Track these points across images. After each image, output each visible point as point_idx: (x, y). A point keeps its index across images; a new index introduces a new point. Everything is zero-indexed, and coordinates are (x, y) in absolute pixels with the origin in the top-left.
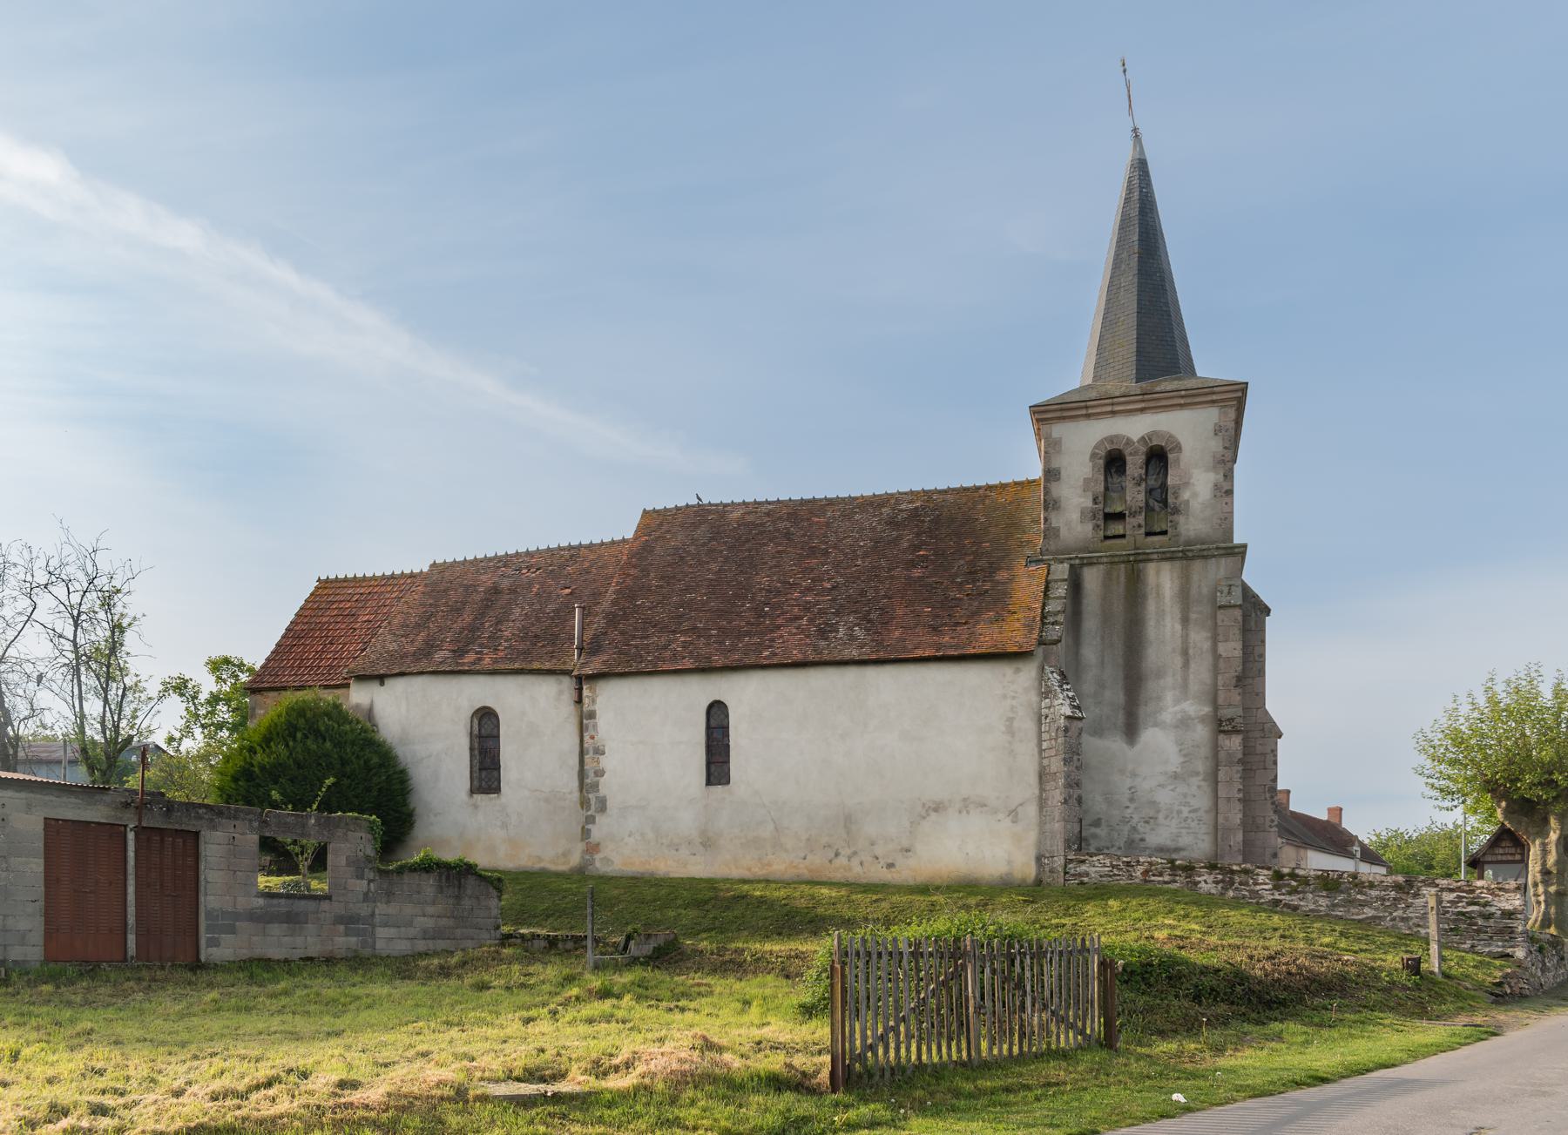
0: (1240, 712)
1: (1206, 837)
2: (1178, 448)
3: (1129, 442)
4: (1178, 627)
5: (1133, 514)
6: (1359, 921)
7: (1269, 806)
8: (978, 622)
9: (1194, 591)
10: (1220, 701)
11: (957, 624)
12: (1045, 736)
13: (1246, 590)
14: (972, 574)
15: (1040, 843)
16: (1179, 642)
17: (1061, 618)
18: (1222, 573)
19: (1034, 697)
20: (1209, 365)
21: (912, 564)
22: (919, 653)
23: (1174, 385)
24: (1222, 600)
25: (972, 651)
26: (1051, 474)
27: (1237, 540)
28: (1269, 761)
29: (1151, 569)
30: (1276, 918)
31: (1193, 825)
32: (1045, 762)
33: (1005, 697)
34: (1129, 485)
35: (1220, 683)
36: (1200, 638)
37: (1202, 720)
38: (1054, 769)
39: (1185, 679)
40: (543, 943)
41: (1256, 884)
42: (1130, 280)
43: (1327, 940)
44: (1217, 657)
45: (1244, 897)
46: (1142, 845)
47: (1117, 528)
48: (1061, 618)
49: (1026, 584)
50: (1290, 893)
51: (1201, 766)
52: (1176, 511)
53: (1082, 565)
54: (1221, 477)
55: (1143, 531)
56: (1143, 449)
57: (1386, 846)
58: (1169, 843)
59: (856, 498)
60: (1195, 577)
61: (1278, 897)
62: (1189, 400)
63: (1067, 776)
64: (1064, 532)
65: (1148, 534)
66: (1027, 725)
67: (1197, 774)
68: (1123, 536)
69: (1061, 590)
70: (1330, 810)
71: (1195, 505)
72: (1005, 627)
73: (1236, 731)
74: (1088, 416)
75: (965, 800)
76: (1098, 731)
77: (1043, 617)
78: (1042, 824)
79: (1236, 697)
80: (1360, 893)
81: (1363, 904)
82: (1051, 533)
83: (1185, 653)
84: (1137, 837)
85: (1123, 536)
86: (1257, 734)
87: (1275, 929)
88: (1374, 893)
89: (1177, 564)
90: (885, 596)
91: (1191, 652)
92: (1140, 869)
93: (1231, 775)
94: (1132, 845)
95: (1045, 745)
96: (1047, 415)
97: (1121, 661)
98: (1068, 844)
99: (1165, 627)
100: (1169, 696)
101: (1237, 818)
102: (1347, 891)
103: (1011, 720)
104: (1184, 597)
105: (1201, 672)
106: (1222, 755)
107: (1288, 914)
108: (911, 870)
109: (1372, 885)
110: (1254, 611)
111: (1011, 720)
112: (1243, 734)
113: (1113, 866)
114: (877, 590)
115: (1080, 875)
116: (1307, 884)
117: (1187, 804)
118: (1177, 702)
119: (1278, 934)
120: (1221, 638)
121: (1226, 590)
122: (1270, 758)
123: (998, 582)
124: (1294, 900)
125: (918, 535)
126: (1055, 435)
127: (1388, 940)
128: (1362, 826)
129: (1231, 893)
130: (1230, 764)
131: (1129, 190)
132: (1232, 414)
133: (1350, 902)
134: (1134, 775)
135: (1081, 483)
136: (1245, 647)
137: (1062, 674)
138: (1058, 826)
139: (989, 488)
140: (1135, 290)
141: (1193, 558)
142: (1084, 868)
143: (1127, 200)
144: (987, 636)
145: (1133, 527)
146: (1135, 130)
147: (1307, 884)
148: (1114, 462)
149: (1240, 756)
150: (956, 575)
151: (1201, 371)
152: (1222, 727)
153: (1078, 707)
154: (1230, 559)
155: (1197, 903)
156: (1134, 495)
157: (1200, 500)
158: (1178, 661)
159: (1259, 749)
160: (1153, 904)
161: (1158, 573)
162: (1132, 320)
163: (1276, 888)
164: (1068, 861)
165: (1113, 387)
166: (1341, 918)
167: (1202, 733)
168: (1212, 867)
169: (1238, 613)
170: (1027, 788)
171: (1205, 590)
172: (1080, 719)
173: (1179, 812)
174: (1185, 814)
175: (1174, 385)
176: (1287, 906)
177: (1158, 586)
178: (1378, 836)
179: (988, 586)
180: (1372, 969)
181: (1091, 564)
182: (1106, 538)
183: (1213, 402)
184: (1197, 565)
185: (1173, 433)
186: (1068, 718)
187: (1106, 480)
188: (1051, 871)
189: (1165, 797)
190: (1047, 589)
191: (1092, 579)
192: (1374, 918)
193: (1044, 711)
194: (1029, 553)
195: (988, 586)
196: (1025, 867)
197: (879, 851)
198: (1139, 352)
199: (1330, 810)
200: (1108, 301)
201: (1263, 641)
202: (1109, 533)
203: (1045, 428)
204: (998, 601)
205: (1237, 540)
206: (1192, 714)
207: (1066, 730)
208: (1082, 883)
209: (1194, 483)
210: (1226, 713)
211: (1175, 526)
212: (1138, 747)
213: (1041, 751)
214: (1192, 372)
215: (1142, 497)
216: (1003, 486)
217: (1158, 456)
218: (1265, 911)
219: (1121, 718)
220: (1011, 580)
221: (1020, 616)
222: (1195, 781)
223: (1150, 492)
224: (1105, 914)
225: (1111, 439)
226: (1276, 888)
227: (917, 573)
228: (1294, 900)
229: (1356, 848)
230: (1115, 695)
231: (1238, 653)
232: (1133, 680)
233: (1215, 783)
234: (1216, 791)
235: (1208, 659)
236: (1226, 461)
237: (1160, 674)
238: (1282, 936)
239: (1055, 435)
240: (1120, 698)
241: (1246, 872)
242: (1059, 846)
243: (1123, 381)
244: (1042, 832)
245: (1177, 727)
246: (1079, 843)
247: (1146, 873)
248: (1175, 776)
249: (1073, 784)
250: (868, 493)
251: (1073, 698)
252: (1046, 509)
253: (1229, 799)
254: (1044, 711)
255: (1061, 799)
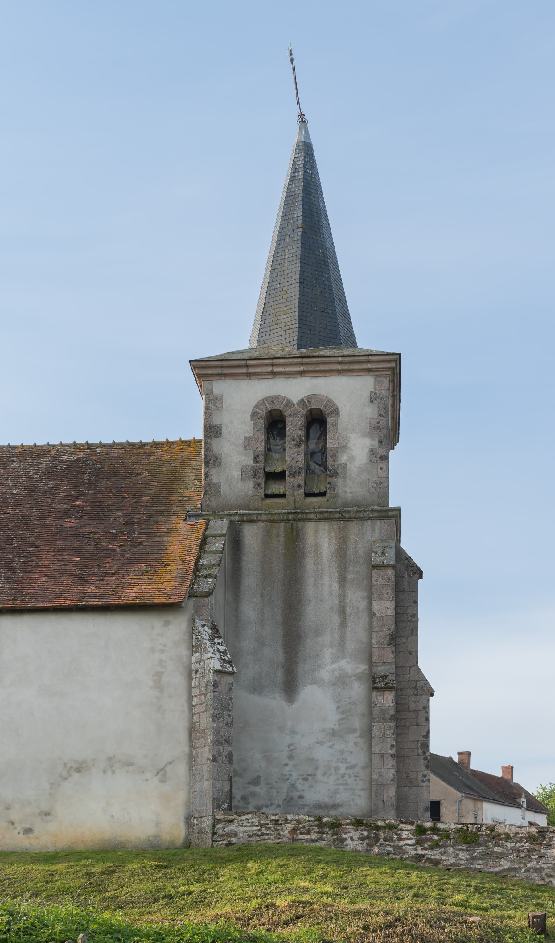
0: (393, 669)
1: (362, 793)
2: (336, 412)
3: (289, 403)
4: (336, 586)
5: (294, 475)
6: (497, 873)
7: (422, 762)
8: (128, 573)
9: (351, 552)
10: (375, 659)
11: (106, 574)
12: (195, 692)
13: (400, 555)
14: (128, 526)
15: (189, 802)
16: (336, 601)
17: (214, 571)
18: (377, 535)
19: (184, 651)
20: (369, 334)
21: (66, 513)
22: (60, 602)
23: (334, 352)
24: (377, 561)
25: (117, 601)
26: (212, 430)
27: (392, 504)
28: (422, 718)
29: (310, 528)
30: (414, 875)
31: (350, 781)
32: (195, 718)
33: (153, 650)
34: (289, 445)
35: (374, 641)
36: (356, 597)
37: (359, 677)
38: (203, 725)
39: (343, 638)
40: (224, 846)
41: (400, 839)
42: (294, 252)
43: (459, 897)
44: (372, 615)
45: (389, 853)
46: (301, 802)
47: (277, 488)
48: (214, 571)
49: (182, 538)
50: (432, 848)
51: (357, 723)
52: (334, 473)
53: (242, 522)
54: (376, 443)
55: (302, 491)
56: (303, 411)
57: (550, 797)
58: (327, 800)
59: (16, 448)
60: (352, 538)
61: (420, 852)
62: (345, 367)
63: (217, 732)
64: (224, 489)
65: (308, 495)
66: (176, 680)
67: (354, 730)
68: (283, 496)
69: (217, 544)
70: (503, 768)
71: (353, 469)
72: (156, 577)
73: (388, 688)
74: (249, 375)
75: (110, 759)
76: (257, 688)
77: (197, 569)
78: (191, 783)
79: (389, 655)
80: (497, 845)
81: (500, 856)
82: (211, 489)
83: (342, 611)
84: (296, 794)
85: (283, 496)
86: (410, 692)
87: (410, 888)
88: (510, 845)
89: (335, 524)
90: (32, 545)
91: (348, 610)
92: (288, 827)
93: (387, 729)
94: (291, 803)
95: (195, 701)
96: (208, 370)
97: (280, 618)
98: (217, 804)
99: (322, 586)
100: (327, 654)
101: (389, 773)
102: (485, 844)
103: (159, 675)
104: (342, 556)
105: (357, 630)
106: (376, 711)
107: (429, 870)
108: (46, 837)
109: (508, 838)
110: (406, 574)
111: (159, 675)
112: (399, 692)
113: (261, 826)
114: (24, 537)
115: (228, 835)
116: (448, 838)
117: (344, 761)
118: (335, 659)
119: (411, 893)
120: (375, 596)
121: (380, 551)
122: (422, 714)
123: (155, 535)
124: (435, 854)
125: (76, 486)
126: (216, 391)
127: (521, 892)
128: (531, 782)
129: (376, 850)
130: (384, 720)
131: (294, 169)
132: (386, 383)
133: (488, 855)
134: (293, 732)
135: (242, 441)
136: (397, 607)
137: (214, 628)
138: (206, 785)
139: (155, 445)
140: (298, 262)
141: (350, 519)
142: (232, 828)
143: (292, 178)
144: (135, 588)
145: (292, 486)
146: (301, 115)
147: (448, 838)
148: (274, 423)
149: (392, 712)
150: (112, 527)
151: (360, 345)
152: (377, 683)
153: (229, 662)
154: (384, 522)
155: (338, 862)
156: (293, 456)
157: (357, 463)
158: (336, 619)
159: (412, 706)
160: (293, 865)
161: (316, 532)
162: (295, 290)
163: (419, 842)
164: (216, 821)
165: (275, 350)
166: (480, 871)
167: (358, 690)
168: (358, 823)
169: (391, 573)
170: (176, 746)
171: (361, 552)
172: (231, 674)
173: (337, 769)
174: (342, 770)
175: (334, 352)
176: (429, 860)
177: (317, 545)
178: (544, 789)
179: (143, 538)
180: (497, 930)
181: (250, 521)
182: (267, 496)
183: (369, 370)
184: (354, 526)
185: (331, 397)
186: (217, 672)
187: (268, 440)
188: (200, 832)
189: (323, 754)
190: (204, 542)
191: (252, 535)
192: (510, 869)
193: (195, 666)
194: (188, 507)
195: (143, 538)
196: (173, 828)
197: (14, 815)
198: (301, 320)
199: (503, 768)
200: (273, 270)
201: (416, 602)
202: (270, 492)
203: (206, 384)
204: (151, 552)
205: (392, 504)
206: (350, 672)
207: (216, 685)
208: (230, 844)
209: (353, 447)
210: (381, 670)
211: (333, 487)
212: (297, 704)
213: (191, 707)
214: (354, 344)
215: (301, 458)
216: (169, 444)
217: (318, 420)
218: (406, 867)
219: (280, 675)
220: (168, 533)
221: (173, 568)
222: (352, 738)
223: (310, 455)
224: (242, 878)
225: (272, 400)
226: (419, 842)
227: (70, 522)
228: (435, 854)
229: (523, 800)
230: (274, 652)
231: (391, 612)
232: (292, 638)
233: (370, 738)
234: (370, 747)
235: (365, 617)
236: (388, 433)
237: (318, 632)
238: (416, 896)
239: (216, 391)
240: (280, 656)
241: (390, 827)
242: (208, 805)
243: (286, 342)
244: (191, 792)
245: (334, 684)
246: (228, 803)
247: (294, 831)
248: (333, 734)
249: (222, 741)
250: (28, 442)
251: (224, 653)
252: (207, 464)
253: (382, 755)
254: (195, 666)
255: (210, 756)
